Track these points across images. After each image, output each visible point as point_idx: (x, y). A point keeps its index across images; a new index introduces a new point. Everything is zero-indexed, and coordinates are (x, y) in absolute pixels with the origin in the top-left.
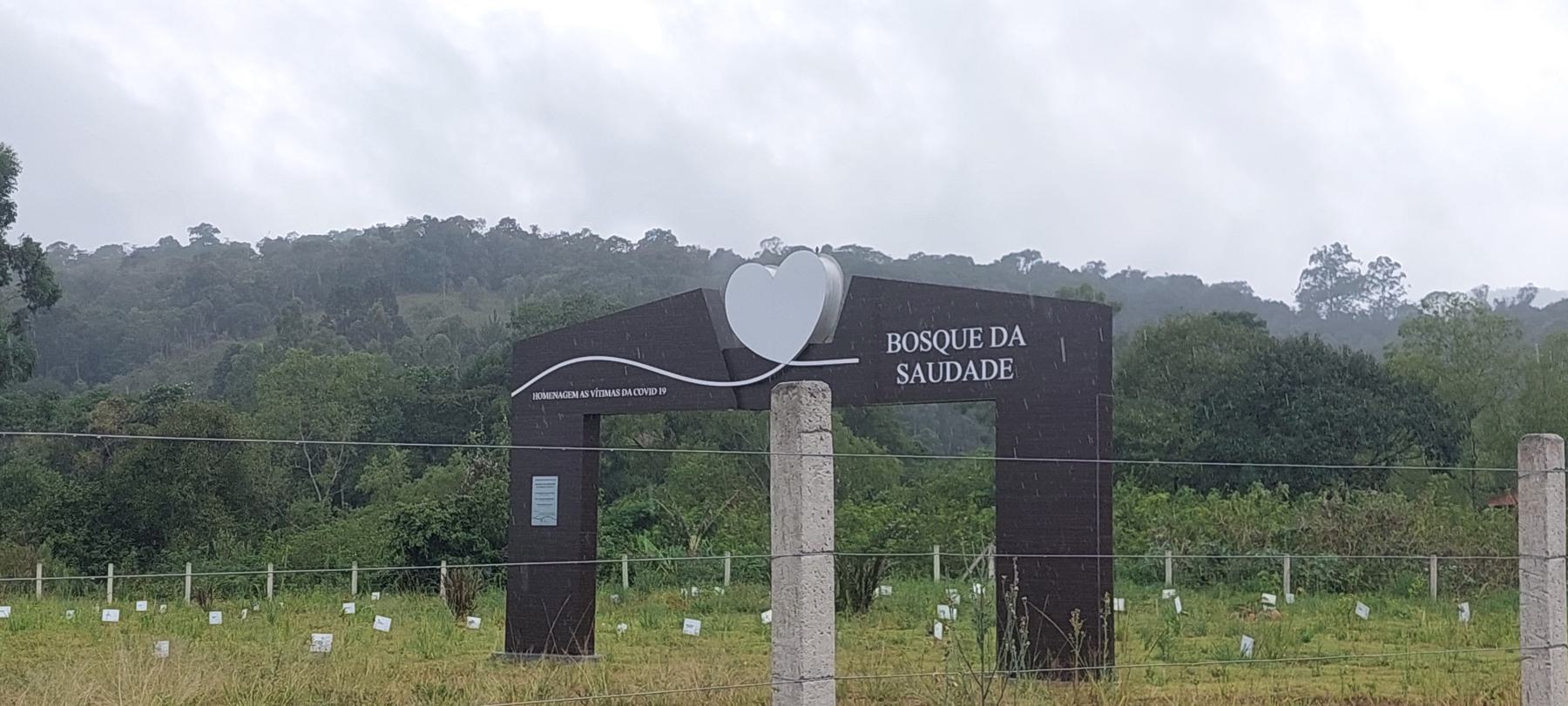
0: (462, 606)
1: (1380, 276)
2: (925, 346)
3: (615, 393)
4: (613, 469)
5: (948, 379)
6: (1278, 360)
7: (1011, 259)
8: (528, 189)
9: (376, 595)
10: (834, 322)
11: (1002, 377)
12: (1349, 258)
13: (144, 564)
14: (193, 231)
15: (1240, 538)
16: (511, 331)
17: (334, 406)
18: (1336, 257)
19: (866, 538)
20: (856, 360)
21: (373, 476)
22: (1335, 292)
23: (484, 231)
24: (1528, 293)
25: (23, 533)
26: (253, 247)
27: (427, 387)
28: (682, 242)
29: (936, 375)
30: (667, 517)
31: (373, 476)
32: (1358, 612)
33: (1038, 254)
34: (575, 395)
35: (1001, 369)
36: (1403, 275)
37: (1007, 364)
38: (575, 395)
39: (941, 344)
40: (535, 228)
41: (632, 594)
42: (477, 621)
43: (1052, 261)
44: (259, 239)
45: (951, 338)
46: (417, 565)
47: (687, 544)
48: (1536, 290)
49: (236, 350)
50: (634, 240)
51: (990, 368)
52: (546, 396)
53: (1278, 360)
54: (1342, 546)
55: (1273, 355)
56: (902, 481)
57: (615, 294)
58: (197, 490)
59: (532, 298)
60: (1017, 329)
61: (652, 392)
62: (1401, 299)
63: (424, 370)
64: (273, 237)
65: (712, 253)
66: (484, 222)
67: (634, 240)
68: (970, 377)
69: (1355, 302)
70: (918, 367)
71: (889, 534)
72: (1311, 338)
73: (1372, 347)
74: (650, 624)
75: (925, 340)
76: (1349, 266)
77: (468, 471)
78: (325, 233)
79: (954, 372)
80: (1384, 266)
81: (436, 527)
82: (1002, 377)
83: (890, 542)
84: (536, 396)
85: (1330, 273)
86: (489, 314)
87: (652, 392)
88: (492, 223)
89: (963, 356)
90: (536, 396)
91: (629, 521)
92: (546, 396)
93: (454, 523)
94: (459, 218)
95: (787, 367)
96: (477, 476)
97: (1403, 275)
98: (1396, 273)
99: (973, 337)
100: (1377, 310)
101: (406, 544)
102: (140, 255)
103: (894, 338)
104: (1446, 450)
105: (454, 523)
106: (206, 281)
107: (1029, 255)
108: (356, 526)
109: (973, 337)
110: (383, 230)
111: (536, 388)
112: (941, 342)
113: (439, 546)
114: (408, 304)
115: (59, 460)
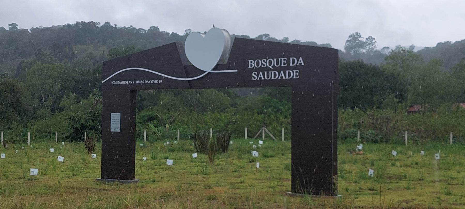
0: (90, 149)
1: (369, 42)
2: (264, 65)
3: (142, 82)
4: (141, 100)
5: (273, 78)
6: (350, 68)
7: (261, 36)
9: (63, 143)
10: (227, 56)
11: (295, 77)
12: (360, 37)
14: (10, 25)
15: (342, 125)
16: (108, 57)
17: (51, 81)
18: (356, 36)
19: (223, 125)
20: (236, 71)
21: (65, 102)
23: (100, 26)
24: (412, 47)
26: (29, 30)
27: (82, 74)
28: (161, 30)
29: (268, 77)
30: (158, 117)
31: (65, 102)
32: (393, 153)
33: (269, 35)
34: (127, 82)
35: (294, 74)
36: (376, 42)
37: (296, 72)
38: (127, 82)
39: (270, 65)
40: (116, 25)
41: (148, 144)
42: (95, 155)
43: (273, 37)
44: (30, 28)
45: (274, 62)
46: (75, 135)
47: (165, 127)
48: (414, 46)
49: (23, 62)
50: (146, 29)
51: (289, 74)
52: (115, 83)
53: (350, 68)
54: (375, 128)
55: (349, 66)
56: (232, 106)
57: (141, 46)
58: (7, 107)
59: (115, 47)
60: (301, 59)
61: (156, 82)
62: (375, 49)
63: (81, 69)
64: (35, 27)
65: (171, 33)
66: (100, 23)
67: (146, 29)
68: (282, 77)
69: (362, 50)
70: (261, 73)
71: (229, 123)
72: (360, 61)
73: (377, 63)
74: (154, 158)
75: (264, 63)
76: (360, 39)
77: (94, 102)
78: (51, 26)
79: (274, 76)
81: (83, 121)
82: (295, 77)
83: (230, 126)
84: (112, 83)
85: (354, 40)
86: (101, 52)
87: (156, 82)
88: (102, 23)
89: (279, 69)
90: (112, 83)
91: (146, 118)
92: (115, 83)
93: (89, 119)
94: (92, 22)
95: (209, 73)
96: (97, 104)
97: (376, 42)
98: (374, 41)
99: (283, 61)
100: (368, 51)
101: (73, 126)
103: (251, 62)
104: (402, 97)
105: (89, 119)
107: (266, 35)
108: (59, 119)
109: (283, 61)
110: (69, 25)
111: (113, 79)
114: (76, 49)
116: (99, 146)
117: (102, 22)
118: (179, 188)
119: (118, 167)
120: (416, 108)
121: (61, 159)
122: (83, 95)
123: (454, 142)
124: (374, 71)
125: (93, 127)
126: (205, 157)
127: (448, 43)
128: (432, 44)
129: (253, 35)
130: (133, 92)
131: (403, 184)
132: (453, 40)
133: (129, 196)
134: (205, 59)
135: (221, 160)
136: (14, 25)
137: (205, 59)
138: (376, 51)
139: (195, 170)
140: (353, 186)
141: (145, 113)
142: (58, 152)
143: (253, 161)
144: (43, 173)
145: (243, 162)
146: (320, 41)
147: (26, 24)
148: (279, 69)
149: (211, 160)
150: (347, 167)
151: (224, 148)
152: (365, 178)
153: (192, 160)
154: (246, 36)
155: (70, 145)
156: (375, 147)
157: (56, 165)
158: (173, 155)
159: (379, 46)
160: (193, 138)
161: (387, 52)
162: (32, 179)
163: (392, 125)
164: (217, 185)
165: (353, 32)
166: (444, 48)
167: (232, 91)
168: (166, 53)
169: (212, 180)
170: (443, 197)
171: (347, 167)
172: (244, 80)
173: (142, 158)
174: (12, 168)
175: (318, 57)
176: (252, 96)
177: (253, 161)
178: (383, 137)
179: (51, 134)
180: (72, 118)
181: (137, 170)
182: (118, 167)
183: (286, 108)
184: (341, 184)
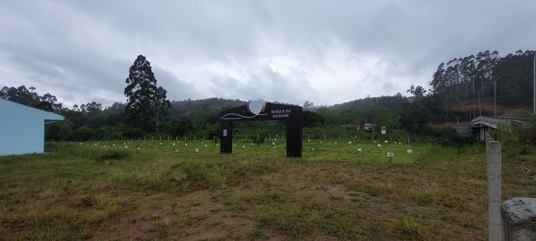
0: (216, 142)
8: (229, 95)
13: (181, 136)
21: (207, 126)
25: (322, 208)
31: (207, 126)
35: (287, 115)
46: (211, 137)
73: (315, 111)
75: (277, 112)
80: (312, 103)
86: (219, 108)
89: (282, 114)
106: (189, 105)
113: (214, 134)
114: (211, 107)
115: (173, 124)
116: (219, 141)
118: (247, 156)
119: (226, 148)
120: (328, 127)
121: (206, 146)
122: (213, 123)
124: (313, 114)
125: (217, 134)
126: (256, 144)
129: (272, 102)
130: (231, 122)
131: (324, 153)
132: (348, 102)
133: (231, 159)
134: (256, 110)
135: (262, 146)
137: (256, 110)
139: (253, 149)
140: (307, 154)
141: (234, 129)
142: (205, 143)
143: (273, 146)
144: (200, 151)
145: (269, 146)
146: (295, 104)
147: (194, 99)
149: (258, 146)
150: (305, 147)
151: (263, 142)
152: (311, 151)
153: (252, 146)
155: (209, 141)
156: (314, 140)
157: (204, 148)
158: (245, 144)
159: (315, 106)
160: (252, 138)
161: (318, 108)
162: (197, 153)
164: (261, 154)
166: (337, 106)
167: (265, 121)
168: (241, 109)
169: (259, 153)
170: (338, 157)
171: (305, 147)
172: (270, 117)
173: (234, 145)
174: (189, 149)
175: (295, 110)
176: (272, 123)
177: (273, 146)
178: (317, 137)
179: (202, 137)
180: (210, 131)
181: (233, 149)
182: (226, 148)
183: (285, 127)
184: (303, 153)
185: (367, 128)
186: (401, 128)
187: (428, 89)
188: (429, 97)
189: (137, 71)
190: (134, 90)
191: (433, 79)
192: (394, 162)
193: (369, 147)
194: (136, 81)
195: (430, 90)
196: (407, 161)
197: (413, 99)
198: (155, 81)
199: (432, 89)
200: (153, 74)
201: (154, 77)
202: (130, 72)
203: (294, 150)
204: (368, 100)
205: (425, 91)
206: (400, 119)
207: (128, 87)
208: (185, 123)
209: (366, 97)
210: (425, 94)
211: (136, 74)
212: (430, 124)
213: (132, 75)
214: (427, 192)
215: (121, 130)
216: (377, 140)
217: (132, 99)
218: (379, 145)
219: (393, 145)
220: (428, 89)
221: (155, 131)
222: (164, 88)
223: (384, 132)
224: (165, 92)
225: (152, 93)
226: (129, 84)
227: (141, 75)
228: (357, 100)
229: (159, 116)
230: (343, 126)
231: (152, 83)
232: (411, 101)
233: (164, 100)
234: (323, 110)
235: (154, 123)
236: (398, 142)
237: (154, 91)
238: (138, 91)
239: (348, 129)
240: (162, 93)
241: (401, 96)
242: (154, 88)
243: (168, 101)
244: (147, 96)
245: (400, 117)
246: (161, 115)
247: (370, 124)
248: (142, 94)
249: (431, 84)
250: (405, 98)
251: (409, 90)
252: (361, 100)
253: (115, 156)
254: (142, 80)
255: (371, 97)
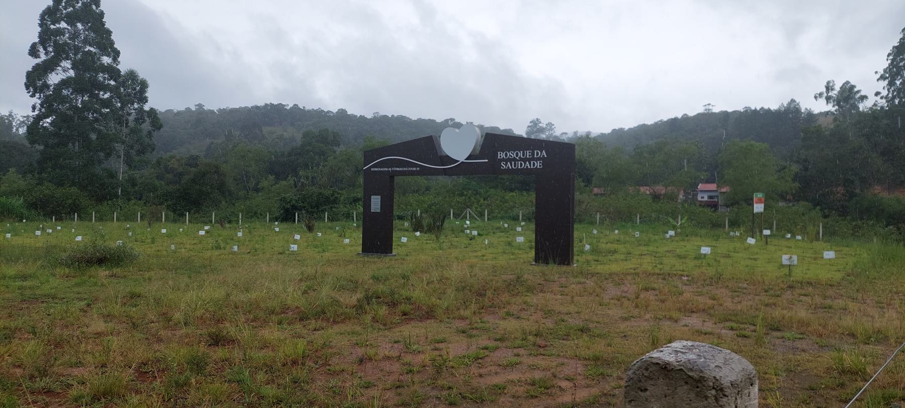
10: (479, 148)
22: (536, 132)
24: (588, 134)
31: (264, 183)
35: (538, 165)
49: (212, 143)
71: (433, 204)
75: (512, 154)
79: (520, 165)
81: (294, 202)
86: (294, 135)
88: (291, 105)
89: (525, 160)
100: (547, 137)
102: (179, 113)
106: (199, 120)
107: (452, 120)
111: (373, 166)
112: (517, 155)
114: (266, 130)
117: (290, 105)
119: (377, 241)
123: (488, 219)
127: (621, 130)
128: (607, 130)
130: (392, 176)
132: (650, 122)
134: (458, 148)
136: (200, 106)
137: (458, 148)
138: (555, 137)
147: (213, 104)
148: (525, 160)
154: (492, 128)
155: (285, 225)
163: (584, 207)
165: (534, 118)
166: (618, 134)
168: (417, 148)
185: (703, 197)
186: (797, 197)
187: (873, 92)
188: (875, 115)
189: (63, 25)
190: (54, 78)
191: (886, 64)
192: (798, 274)
193: (724, 246)
194: (61, 52)
195: (877, 94)
196: (824, 275)
197: (830, 119)
198: (116, 54)
199: (884, 93)
200: (109, 33)
201: (112, 43)
202: (41, 25)
203: (554, 245)
204: (708, 122)
205: (864, 98)
206: (796, 175)
207: (36, 68)
208: (204, 174)
209: (701, 110)
210: (863, 106)
211: (60, 32)
212: (877, 189)
213: (46, 36)
214: (877, 325)
215: (20, 192)
216: (742, 229)
217: (48, 106)
218: (751, 241)
219: (783, 243)
220: (873, 92)
221: (117, 196)
222: (142, 75)
223: (758, 208)
224: (144, 85)
225: (106, 88)
226: (38, 61)
227: (75, 36)
228: (676, 119)
229: (127, 155)
230: (642, 189)
231: (106, 60)
232: (826, 123)
233: (141, 111)
234: (588, 141)
235: (112, 175)
236: (793, 236)
237: (112, 83)
238: (64, 83)
239: (656, 197)
240: (134, 87)
241: (797, 110)
242: (113, 72)
243: (152, 111)
244: (92, 96)
245: (795, 168)
246: (133, 152)
247: (713, 187)
248: (79, 91)
249: (882, 78)
250: (810, 115)
251: (821, 95)
252: (685, 118)
253: (104, 259)
254: (77, 50)
255: (716, 110)
